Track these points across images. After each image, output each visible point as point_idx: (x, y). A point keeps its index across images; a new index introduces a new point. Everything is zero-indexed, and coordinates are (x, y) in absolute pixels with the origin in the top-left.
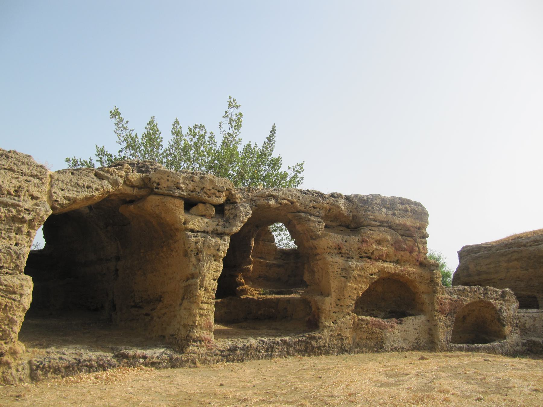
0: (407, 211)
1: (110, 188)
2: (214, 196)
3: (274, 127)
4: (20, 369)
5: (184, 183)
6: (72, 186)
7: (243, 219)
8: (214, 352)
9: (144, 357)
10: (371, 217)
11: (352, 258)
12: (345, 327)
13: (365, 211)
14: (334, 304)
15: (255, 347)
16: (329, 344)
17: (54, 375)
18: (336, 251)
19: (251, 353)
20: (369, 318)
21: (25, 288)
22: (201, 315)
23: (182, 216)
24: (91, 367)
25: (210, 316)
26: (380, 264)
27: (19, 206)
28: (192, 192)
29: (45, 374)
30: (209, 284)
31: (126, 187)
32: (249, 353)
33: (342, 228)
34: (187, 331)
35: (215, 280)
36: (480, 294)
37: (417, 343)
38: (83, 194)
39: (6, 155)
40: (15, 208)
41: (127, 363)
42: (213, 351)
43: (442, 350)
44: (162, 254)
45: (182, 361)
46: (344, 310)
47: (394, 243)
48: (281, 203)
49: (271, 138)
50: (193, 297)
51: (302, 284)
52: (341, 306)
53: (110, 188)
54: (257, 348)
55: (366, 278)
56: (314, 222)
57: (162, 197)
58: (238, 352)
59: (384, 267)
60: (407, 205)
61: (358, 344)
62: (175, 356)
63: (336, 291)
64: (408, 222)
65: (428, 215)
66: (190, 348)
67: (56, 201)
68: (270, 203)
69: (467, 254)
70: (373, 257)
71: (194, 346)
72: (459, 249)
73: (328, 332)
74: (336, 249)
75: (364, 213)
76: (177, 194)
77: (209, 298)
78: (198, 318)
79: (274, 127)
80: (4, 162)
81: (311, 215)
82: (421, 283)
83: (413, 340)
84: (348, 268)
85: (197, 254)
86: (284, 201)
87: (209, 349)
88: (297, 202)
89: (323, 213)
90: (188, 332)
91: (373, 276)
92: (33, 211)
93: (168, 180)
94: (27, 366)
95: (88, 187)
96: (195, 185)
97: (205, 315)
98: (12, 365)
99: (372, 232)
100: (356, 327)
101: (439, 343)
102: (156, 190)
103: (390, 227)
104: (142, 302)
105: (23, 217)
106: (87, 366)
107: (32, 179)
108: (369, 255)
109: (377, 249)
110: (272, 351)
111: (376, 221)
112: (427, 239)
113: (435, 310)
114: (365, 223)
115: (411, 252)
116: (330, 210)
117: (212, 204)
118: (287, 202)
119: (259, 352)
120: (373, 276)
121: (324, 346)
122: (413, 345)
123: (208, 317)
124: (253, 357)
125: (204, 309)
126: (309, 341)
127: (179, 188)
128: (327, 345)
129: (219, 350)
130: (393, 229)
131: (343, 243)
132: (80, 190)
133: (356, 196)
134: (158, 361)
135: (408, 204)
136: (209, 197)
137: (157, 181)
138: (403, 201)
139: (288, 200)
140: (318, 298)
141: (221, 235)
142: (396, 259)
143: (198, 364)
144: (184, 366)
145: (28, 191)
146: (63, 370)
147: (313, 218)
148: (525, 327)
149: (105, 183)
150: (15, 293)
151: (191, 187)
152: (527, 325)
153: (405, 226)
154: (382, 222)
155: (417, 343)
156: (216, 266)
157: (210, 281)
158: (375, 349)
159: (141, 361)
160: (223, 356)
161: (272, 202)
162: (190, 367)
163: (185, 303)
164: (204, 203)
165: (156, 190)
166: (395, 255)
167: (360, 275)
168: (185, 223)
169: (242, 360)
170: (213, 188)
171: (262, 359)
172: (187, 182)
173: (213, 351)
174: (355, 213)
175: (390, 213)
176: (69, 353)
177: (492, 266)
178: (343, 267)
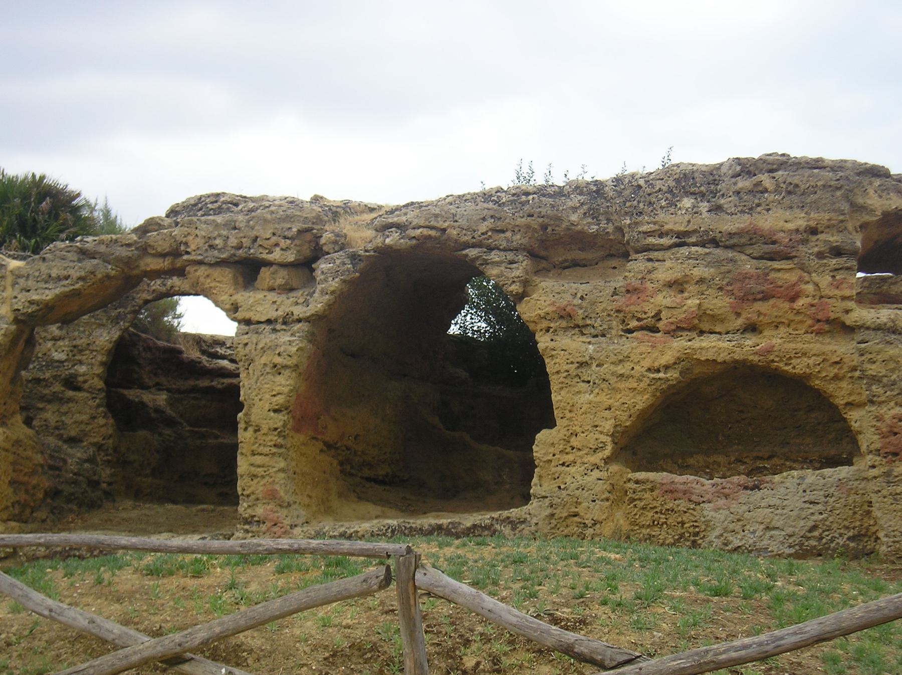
18: (564, 324)
56: (498, 264)
70: (660, 325)
74: (562, 317)
81: (490, 249)
91: (661, 375)
99: (650, 264)
108: (649, 322)
120: (661, 375)
137: (184, 240)
138: (745, 168)
142: (740, 322)
147: (495, 256)
151: (233, 241)
154: (679, 235)
164: (268, 264)
175: (704, 206)
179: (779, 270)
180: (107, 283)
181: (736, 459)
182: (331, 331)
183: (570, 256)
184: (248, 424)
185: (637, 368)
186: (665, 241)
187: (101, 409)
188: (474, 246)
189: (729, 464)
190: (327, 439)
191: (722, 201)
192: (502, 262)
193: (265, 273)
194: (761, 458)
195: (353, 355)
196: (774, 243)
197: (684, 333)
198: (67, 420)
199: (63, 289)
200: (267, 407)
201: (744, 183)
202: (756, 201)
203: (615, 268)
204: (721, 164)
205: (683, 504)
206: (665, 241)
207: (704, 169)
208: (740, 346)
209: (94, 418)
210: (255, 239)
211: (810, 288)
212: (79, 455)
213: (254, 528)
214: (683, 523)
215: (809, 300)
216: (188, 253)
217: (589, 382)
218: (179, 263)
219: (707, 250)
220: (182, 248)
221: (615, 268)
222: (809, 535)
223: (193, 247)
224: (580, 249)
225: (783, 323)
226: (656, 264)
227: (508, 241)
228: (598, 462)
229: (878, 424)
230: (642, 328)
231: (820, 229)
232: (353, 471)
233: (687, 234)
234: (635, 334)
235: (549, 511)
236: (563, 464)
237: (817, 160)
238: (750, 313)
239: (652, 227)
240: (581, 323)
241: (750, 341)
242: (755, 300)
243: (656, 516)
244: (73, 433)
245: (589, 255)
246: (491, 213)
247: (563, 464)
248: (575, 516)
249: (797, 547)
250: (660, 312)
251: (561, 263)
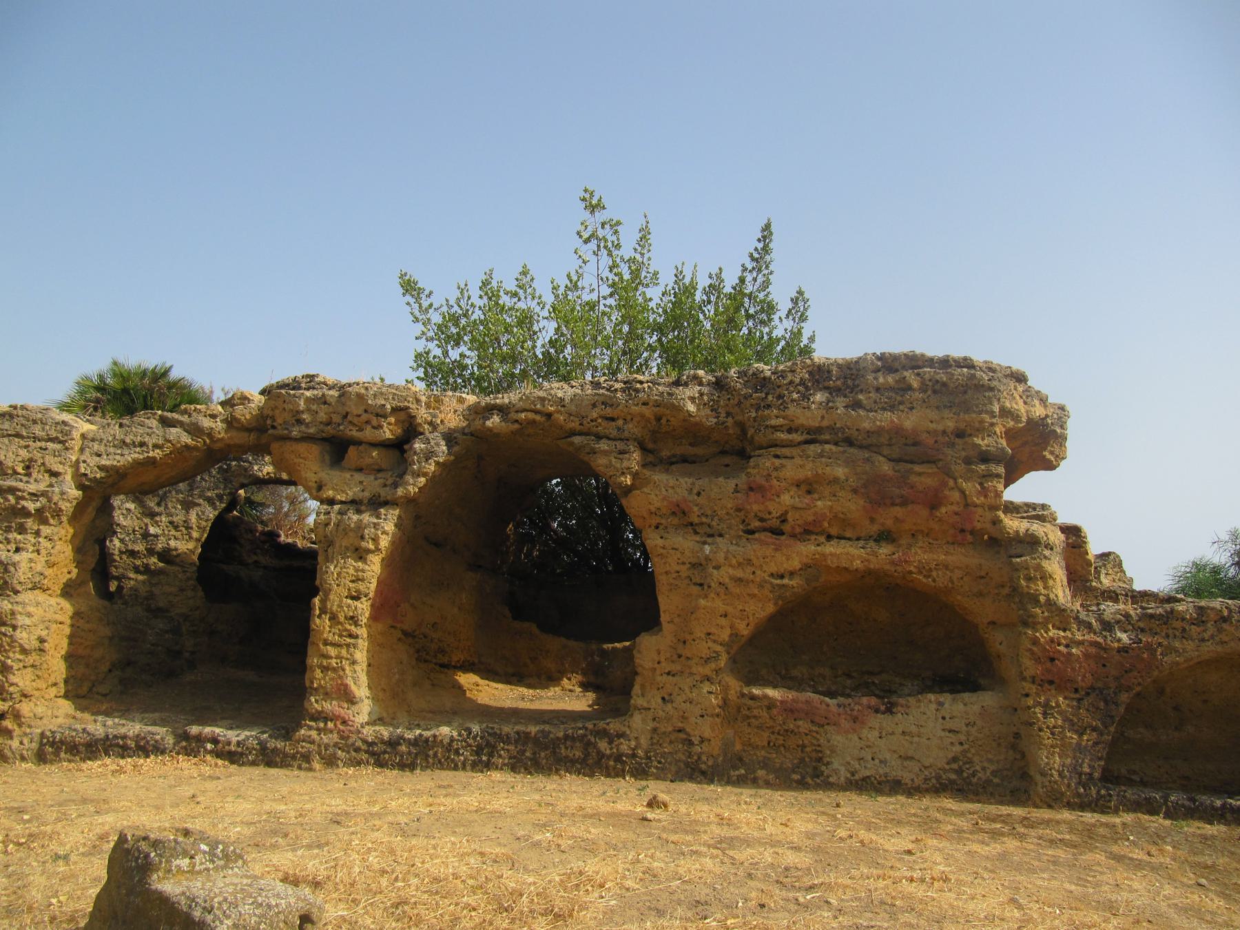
0: (910, 388)
1: (186, 439)
2: (369, 427)
3: (767, 227)
4: (26, 741)
5: (309, 410)
6: (114, 446)
7: (420, 468)
8: (353, 744)
9: (215, 741)
10: (773, 422)
11: (721, 535)
12: (698, 712)
13: (758, 408)
15: (446, 741)
16: (646, 752)
17: (68, 756)
18: (676, 521)
19: (435, 755)
20: (770, 692)
21: (18, 617)
22: (325, 669)
24: (125, 748)
25: (344, 670)
26: (807, 549)
27: (19, 490)
28: (328, 424)
29: (56, 753)
30: (340, 606)
31: (234, 433)
32: (431, 753)
33: (727, 460)
37: (959, 772)
39: (8, 415)
40: (13, 494)
41: (185, 748)
42: (350, 741)
43: (1054, 800)
45: (286, 755)
46: (694, 670)
47: (865, 486)
49: (760, 259)
52: (688, 658)
53: (186, 439)
54: (450, 744)
55: (761, 586)
56: (606, 453)
58: (403, 748)
59: (823, 555)
61: (741, 759)
62: (272, 744)
63: (677, 620)
66: (303, 732)
67: (86, 475)
68: (489, 423)
70: (786, 528)
71: (310, 728)
73: (644, 720)
74: (674, 513)
75: (754, 415)
76: (295, 433)
77: (341, 636)
78: (318, 674)
79: (767, 227)
80: (6, 425)
81: (599, 437)
82: (980, 594)
83: (941, 763)
84: (704, 563)
86: (523, 415)
87: (342, 738)
88: (559, 412)
91: (785, 581)
92: (42, 495)
94: (36, 739)
95: (142, 444)
96: (331, 410)
97: (334, 670)
98: (15, 734)
99: (777, 462)
100: (733, 713)
101: (1038, 778)
105: (23, 507)
106: (118, 745)
108: (775, 523)
109: (795, 508)
110: (491, 755)
113: (1024, 679)
114: (760, 438)
118: (531, 416)
119: (457, 752)
120: (785, 581)
121: (634, 756)
122: (938, 778)
123: (341, 673)
124: (440, 762)
125: (331, 658)
126: (593, 740)
127: (299, 422)
128: (640, 753)
129: (365, 741)
130: (861, 447)
131: (691, 498)
132: (126, 451)
134: (239, 750)
135: (913, 368)
136: (361, 430)
137: (271, 414)
138: (888, 363)
139: (536, 412)
141: (376, 504)
142: (875, 529)
143: (317, 766)
144: (292, 766)
145: (43, 464)
146: (82, 749)
147: (603, 445)
149: (174, 432)
151: (322, 416)
153: (898, 431)
155: (959, 772)
156: (357, 570)
157: (341, 601)
158: (796, 777)
159: (209, 746)
160: (373, 754)
161: (494, 421)
162: (300, 768)
164: (358, 443)
166: (872, 520)
167: (740, 580)
169: (412, 767)
170: (366, 411)
171: (464, 768)
172: (314, 407)
173: (350, 741)
176: (133, 728)
178: (694, 560)
179: (920, 474)
180: (186, 454)
181: (844, 674)
182: (418, 517)
183: (679, 451)
184: (323, 611)
185: (758, 572)
186: (796, 437)
187: (191, 582)
188: (580, 434)
189: (836, 677)
190: (405, 627)
191: (861, 397)
192: (611, 452)
193: (352, 451)
194: (871, 673)
195: (436, 544)
196: (915, 444)
197: (813, 537)
198: (156, 591)
199: (136, 455)
202: (899, 398)
203: (727, 466)
205: (804, 726)
206: (796, 437)
207: (840, 362)
208: (875, 554)
209: (182, 590)
210: (345, 416)
211: (956, 495)
212: (161, 626)
214: (804, 746)
215: (955, 508)
216: (274, 427)
217: (701, 585)
218: (264, 440)
219: (841, 449)
220: (269, 422)
221: (727, 466)
222: (947, 767)
223: (280, 421)
224: (691, 444)
225: (922, 532)
226: (783, 461)
227: (619, 429)
228: (709, 673)
229: (1035, 649)
230: (765, 530)
231: (969, 432)
232: (428, 658)
233: (819, 430)
234: (757, 535)
235: (651, 725)
236: (668, 673)
237: (965, 359)
238: (888, 517)
239: (780, 421)
240: (696, 520)
241: (884, 550)
242: (893, 504)
243: (773, 737)
244: (161, 604)
245: (699, 451)
246: (602, 399)
247: (668, 673)
248: (680, 731)
249: (934, 781)
250: (786, 512)
251: (669, 458)
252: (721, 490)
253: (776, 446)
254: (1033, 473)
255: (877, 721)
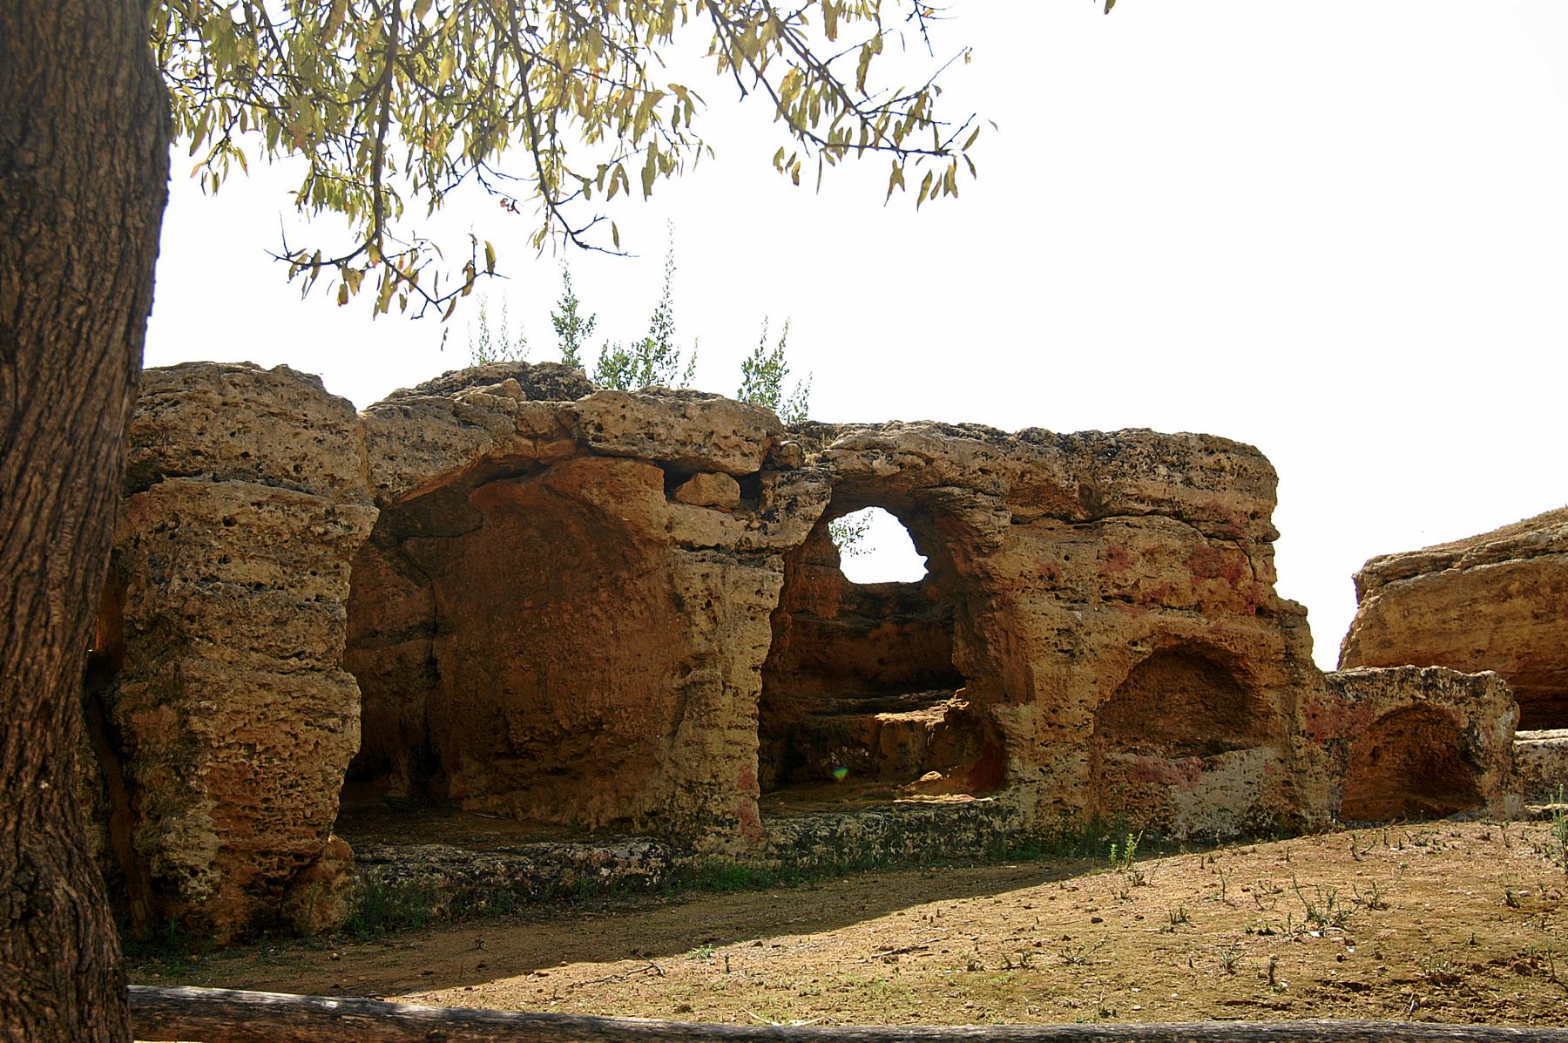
0: (1222, 469)
10: (1128, 491)
14: (1041, 723)
23: (656, 505)
26: (1154, 617)
28: (684, 444)
34: (696, 798)
35: (755, 669)
36: (1418, 687)
38: (429, 471)
44: (595, 609)
48: (901, 465)
50: (708, 713)
51: (941, 680)
52: (1061, 727)
56: (985, 509)
57: (610, 461)
60: (1222, 456)
64: (1230, 499)
65: (1276, 478)
69: (1382, 580)
72: (1358, 567)
74: (1041, 577)
85: (709, 604)
89: (1005, 484)
90: (701, 801)
91: (1139, 648)
93: (624, 417)
102: (595, 445)
103: (1177, 515)
104: (532, 739)
107: (326, 433)
111: (1142, 502)
112: (1275, 544)
115: (1233, 581)
116: (1023, 474)
117: (731, 474)
133: (1086, 436)
135: (1225, 451)
138: (1211, 445)
139: (920, 456)
140: (1000, 709)
141: (754, 555)
147: (981, 499)
148: (1539, 775)
150: (331, 714)
151: (679, 433)
152: (1543, 771)
154: (1157, 502)
163: (688, 730)
164: (713, 469)
165: (595, 445)
167: (1107, 646)
168: (669, 528)
174: (1089, 483)
175: (1178, 477)
177: (1454, 614)
178: (1062, 626)
200: (749, 663)
201: (1209, 461)
204: (830, 431)
213: (727, 830)
235: (1035, 798)
239: (1133, 491)
252: (1086, 558)
253: (1126, 514)
254: (911, 581)
255: (1205, 777)
